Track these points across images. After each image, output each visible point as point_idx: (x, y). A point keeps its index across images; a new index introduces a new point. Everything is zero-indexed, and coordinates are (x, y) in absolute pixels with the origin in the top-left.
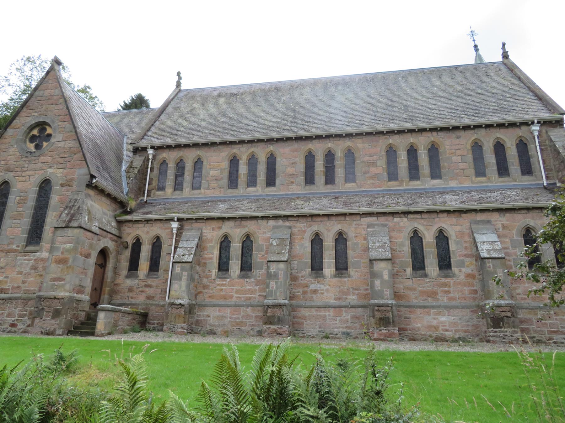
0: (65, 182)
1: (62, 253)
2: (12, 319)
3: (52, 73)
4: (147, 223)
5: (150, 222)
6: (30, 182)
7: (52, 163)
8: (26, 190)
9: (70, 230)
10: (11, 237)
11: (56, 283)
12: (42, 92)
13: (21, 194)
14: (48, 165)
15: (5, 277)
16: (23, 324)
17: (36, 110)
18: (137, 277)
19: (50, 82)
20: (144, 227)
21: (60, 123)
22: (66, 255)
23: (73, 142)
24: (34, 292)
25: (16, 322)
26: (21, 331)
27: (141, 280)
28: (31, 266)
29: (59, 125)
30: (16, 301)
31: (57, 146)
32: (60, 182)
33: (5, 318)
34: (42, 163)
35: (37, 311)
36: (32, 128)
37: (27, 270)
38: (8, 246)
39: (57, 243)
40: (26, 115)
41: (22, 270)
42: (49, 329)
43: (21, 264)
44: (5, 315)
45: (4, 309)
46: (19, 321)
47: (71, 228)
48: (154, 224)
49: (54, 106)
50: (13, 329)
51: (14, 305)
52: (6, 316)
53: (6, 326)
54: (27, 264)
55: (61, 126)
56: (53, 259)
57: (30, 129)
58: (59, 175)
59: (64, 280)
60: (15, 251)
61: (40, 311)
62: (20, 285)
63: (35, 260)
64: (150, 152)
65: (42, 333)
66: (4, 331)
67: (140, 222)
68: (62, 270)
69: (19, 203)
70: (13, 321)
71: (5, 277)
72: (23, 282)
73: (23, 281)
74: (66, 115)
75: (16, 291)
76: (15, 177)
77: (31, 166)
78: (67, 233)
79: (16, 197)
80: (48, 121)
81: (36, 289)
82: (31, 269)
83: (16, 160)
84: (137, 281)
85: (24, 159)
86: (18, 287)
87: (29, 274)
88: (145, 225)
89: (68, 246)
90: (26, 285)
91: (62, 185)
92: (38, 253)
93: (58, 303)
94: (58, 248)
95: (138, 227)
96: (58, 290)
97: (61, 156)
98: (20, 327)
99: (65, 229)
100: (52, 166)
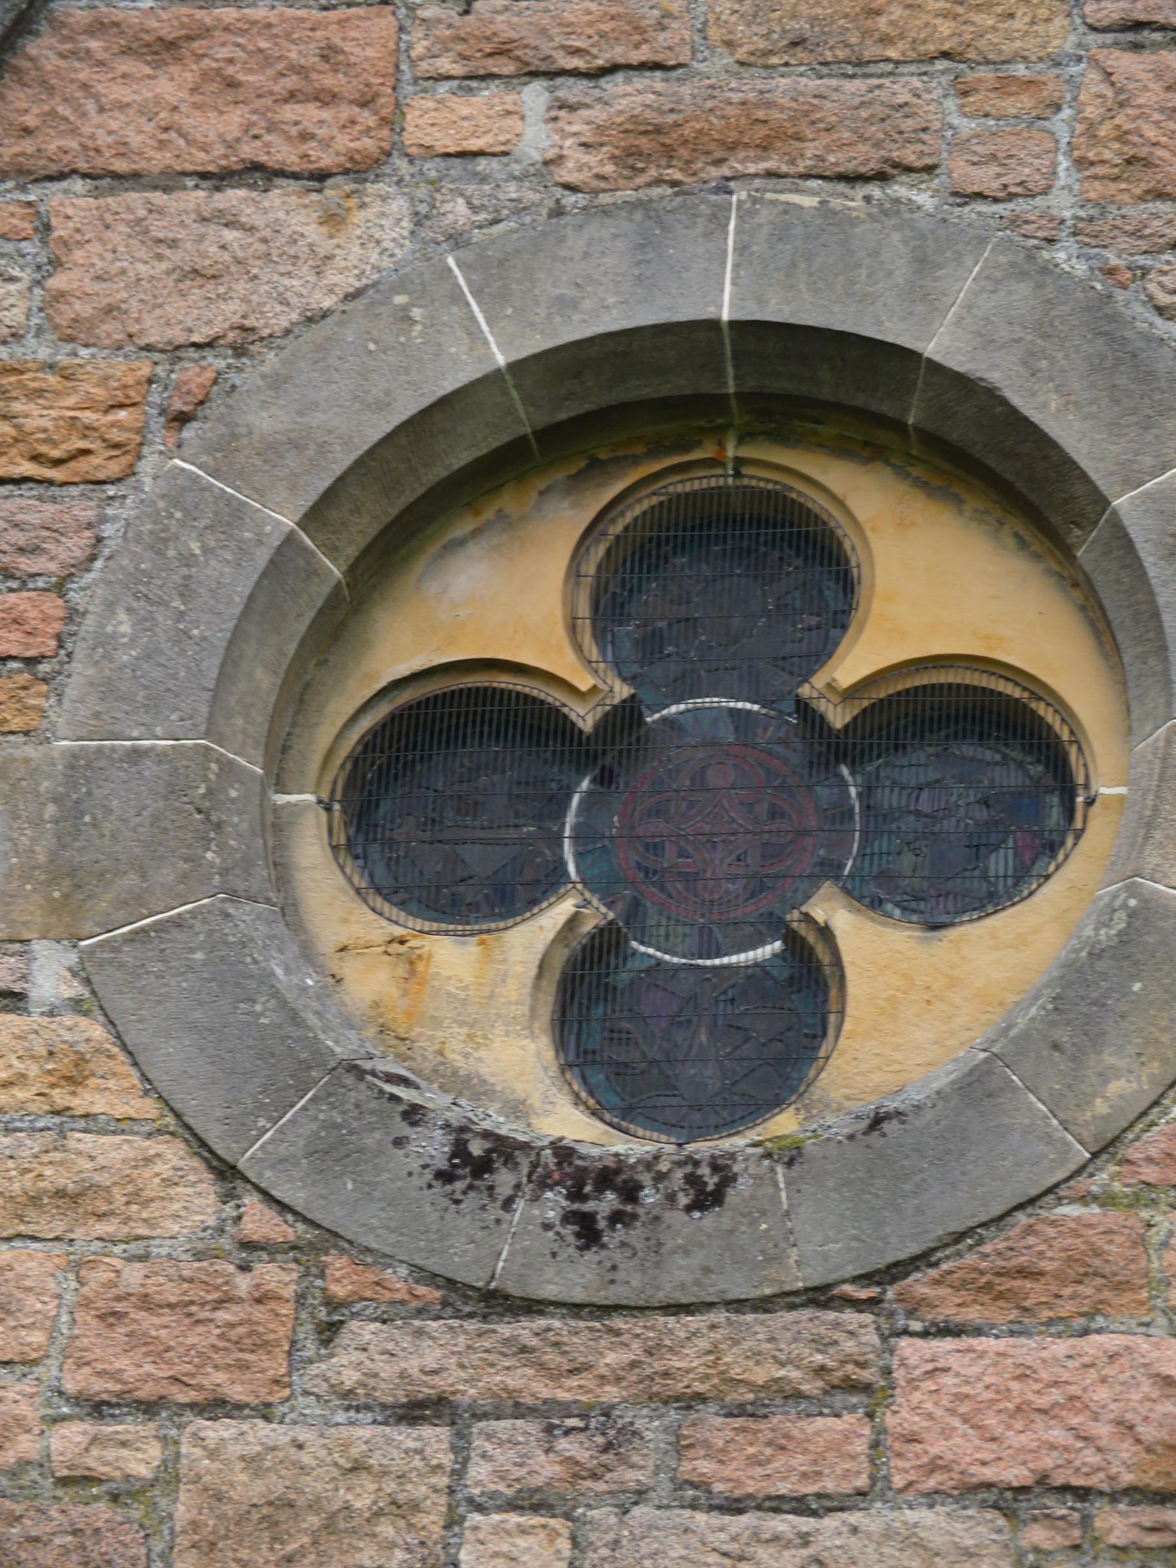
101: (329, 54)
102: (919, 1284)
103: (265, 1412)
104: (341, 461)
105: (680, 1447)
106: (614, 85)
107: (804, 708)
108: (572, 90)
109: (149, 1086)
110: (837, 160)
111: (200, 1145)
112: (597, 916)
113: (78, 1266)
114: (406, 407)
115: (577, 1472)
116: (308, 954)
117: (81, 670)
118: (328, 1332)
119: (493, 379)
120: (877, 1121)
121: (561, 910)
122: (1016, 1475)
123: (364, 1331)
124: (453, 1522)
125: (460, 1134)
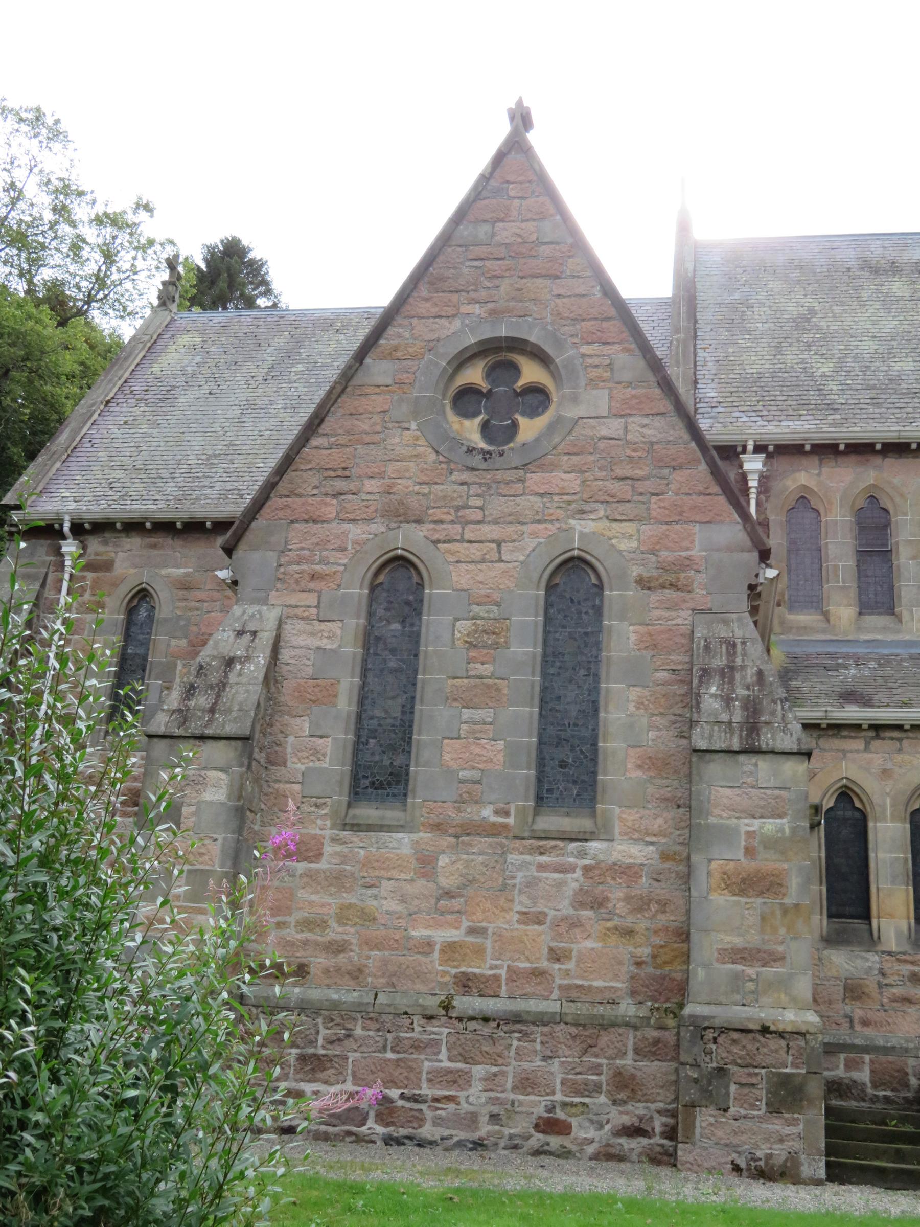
0: (655, 573)
1: (749, 851)
2: (545, 1101)
3: (514, 158)
4: (877, 737)
5: (888, 734)
6: (502, 565)
7: (585, 496)
8: (496, 596)
9: (763, 765)
10: (465, 774)
11: (751, 971)
12: (485, 228)
13: (476, 609)
14: (569, 503)
15: (472, 931)
16: (592, 1122)
17: (472, 295)
18: (871, 941)
19: (512, 194)
20: (867, 749)
21: (585, 349)
22: (768, 862)
23: (659, 422)
24: (608, 995)
25: (560, 1114)
26: (590, 1150)
27: (890, 953)
28: (576, 894)
29: (583, 356)
30: (546, 1029)
31: (589, 432)
32: (635, 571)
33: (512, 1096)
34: (542, 495)
35: (696, 1081)
36: (463, 360)
37: (566, 908)
38: (459, 810)
39: (716, 811)
40: (435, 310)
41: (541, 907)
42: (769, 1157)
43: (531, 883)
44: (509, 1085)
45: (500, 1061)
46: (574, 1110)
47: (768, 757)
48: (905, 743)
49: (548, 282)
50: (555, 1141)
51: (538, 1047)
52: (515, 1088)
53: (520, 1126)
54: (560, 885)
55: (596, 361)
56: (717, 876)
57: (455, 364)
58: (624, 545)
59: (779, 959)
60: (494, 830)
61: (710, 1083)
62: (544, 964)
63: (587, 869)
64: (753, 464)
65: (737, 1169)
66: (515, 1147)
67: (845, 733)
68: (763, 919)
69: (471, 645)
70: (551, 1109)
71: (472, 931)
72: (556, 956)
73: (551, 950)
74: (607, 319)
75: (529, 989)
76: (436, 542)
77: (497, 506)
78: (751, 773)
79: (458, 619)
80: (532, 339)
81: (619, 985)
82: (580, 904)
83: (426, 479)
84: (874, 958)
85: (456, 476)
86: (538, 974)
87: (575, 924)
88: (867, 744)
89: (770, 826)
90: (571, 965)
91: (644, 584)
92: (594, 845)
93: (783, 1052)
94: (727, 835)
95: (845, 752)
96: (764, 1000)
97: (619, 472)
98: (582, 1135)
99: (742, 758)
100: (586, 507)
101: (450, 300)
102: (529, 466)
103: (442, 484)
104: (451, 356)
105: (498, 488)
106: (488, 304)
107: (514, 390)
108: (482, 305)
109: (427, 441)
110: (519, 314)
111: (433, 448)
112: (486, 417)
113: (417, 465)
114: (461, 348)
115: (484, 491)
116: (447, 422)
117: (417, 385)
118: (451, 473)
119: (472, 345)
120: (524, 445)
121: (481, 417)
122: (542, 492)
123: (456, 473)
124: (468, 498)
125: (468, 447)
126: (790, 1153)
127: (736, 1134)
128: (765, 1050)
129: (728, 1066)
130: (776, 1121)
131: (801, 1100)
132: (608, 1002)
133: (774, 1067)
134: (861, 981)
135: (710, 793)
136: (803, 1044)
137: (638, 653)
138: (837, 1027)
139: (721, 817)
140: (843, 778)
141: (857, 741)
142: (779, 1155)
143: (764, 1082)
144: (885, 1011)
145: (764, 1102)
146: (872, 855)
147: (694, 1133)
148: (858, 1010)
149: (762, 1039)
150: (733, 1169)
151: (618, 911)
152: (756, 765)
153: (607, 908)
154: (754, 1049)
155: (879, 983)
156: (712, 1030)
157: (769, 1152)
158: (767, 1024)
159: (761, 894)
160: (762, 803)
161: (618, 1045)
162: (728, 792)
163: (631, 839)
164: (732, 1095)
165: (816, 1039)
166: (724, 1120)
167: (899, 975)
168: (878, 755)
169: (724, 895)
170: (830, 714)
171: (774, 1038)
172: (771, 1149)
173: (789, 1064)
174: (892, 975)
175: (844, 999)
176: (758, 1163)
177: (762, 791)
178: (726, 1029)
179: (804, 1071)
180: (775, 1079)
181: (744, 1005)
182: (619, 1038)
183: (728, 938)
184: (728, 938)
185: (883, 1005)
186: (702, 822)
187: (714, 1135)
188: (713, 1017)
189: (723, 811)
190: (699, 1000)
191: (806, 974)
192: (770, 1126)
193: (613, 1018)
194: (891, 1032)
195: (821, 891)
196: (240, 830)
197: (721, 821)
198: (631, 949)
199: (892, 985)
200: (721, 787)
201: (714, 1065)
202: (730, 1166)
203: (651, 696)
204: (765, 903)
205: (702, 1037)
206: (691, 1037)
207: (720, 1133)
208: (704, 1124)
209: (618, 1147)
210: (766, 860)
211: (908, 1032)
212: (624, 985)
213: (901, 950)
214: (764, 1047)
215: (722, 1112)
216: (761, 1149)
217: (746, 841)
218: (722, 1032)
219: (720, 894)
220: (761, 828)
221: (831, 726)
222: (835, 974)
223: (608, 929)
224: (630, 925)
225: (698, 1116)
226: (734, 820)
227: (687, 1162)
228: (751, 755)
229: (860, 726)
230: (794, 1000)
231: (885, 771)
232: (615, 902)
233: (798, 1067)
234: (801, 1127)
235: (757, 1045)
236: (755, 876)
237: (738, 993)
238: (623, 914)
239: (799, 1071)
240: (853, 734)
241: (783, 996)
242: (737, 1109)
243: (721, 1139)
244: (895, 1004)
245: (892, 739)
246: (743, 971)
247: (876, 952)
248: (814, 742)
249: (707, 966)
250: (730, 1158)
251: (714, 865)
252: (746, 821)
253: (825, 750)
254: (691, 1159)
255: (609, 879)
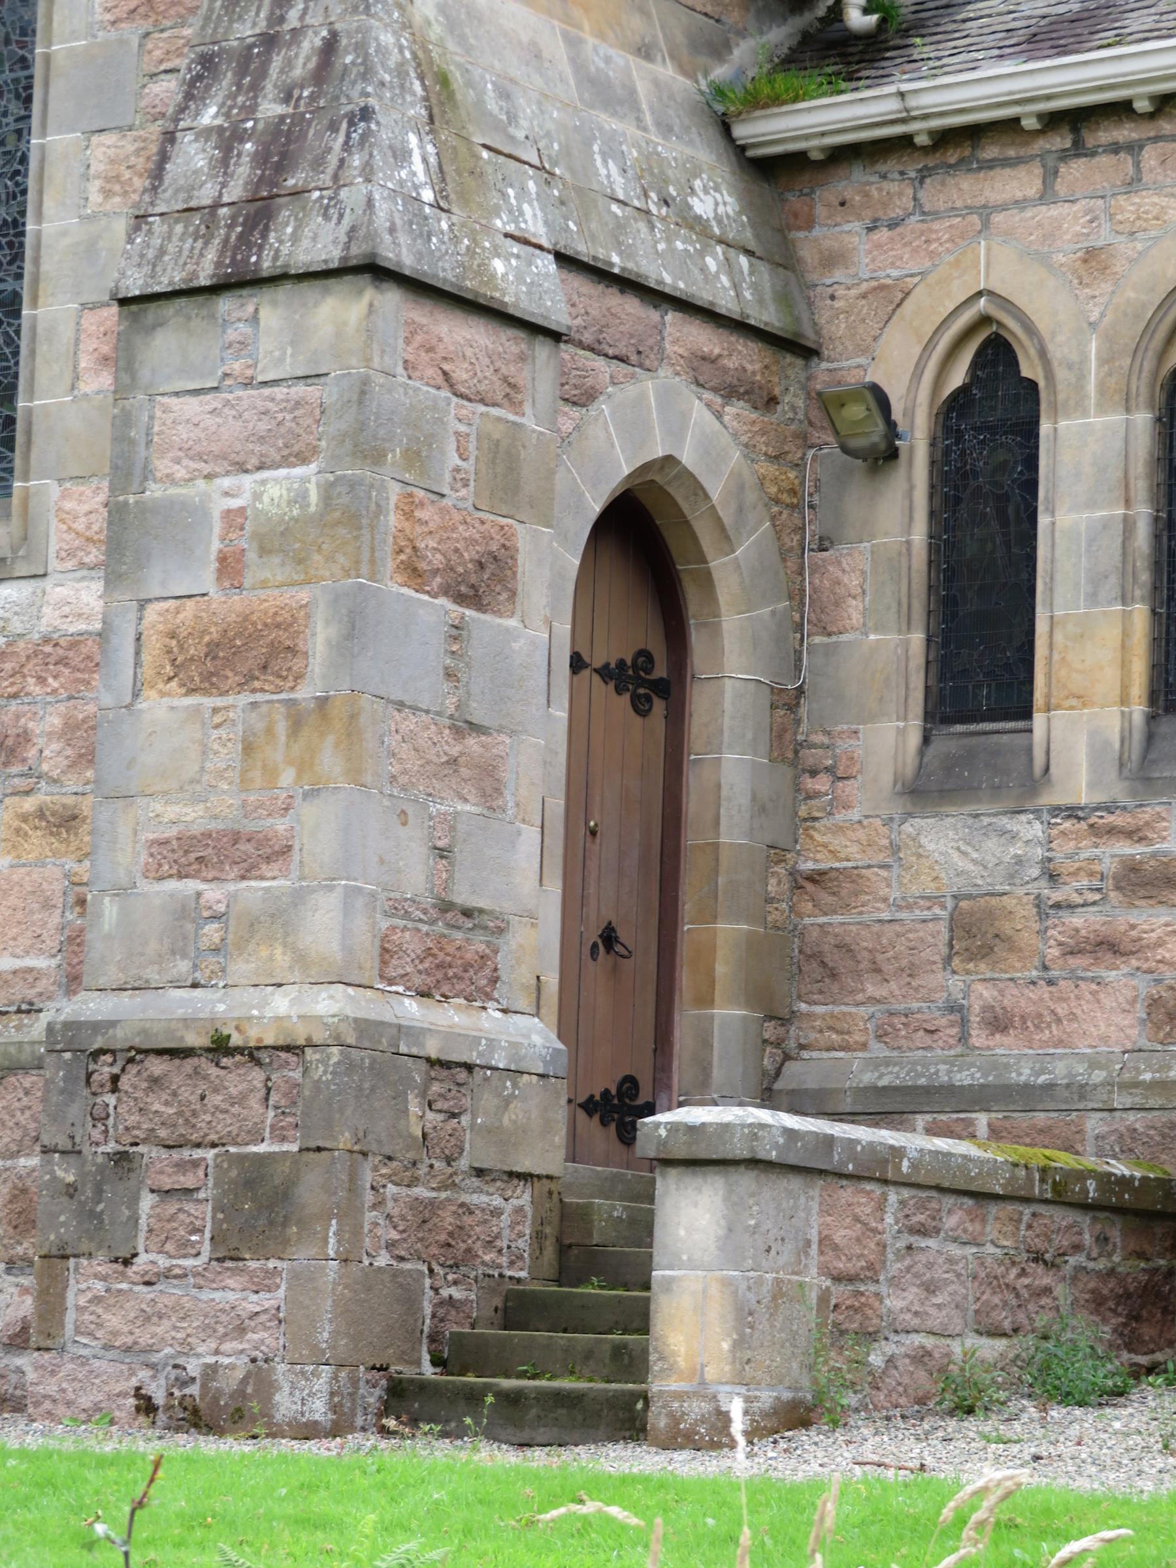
4: (1079, 150)
11: (214, 894)
20: (1047, 195)
27: (1072, 812)
35: (71, 1191)
39: (162, 466)
42: (211, 1371)
47: (283, 292)
48: (1150, 156)
56: (154, 645)
65: (146, 1407)
67: (990, 152)
68: (248, 749)
84: (1030, 829)
88: (1050, 176)
93: (255, 1102)
95: (986, 212)
96: (241, 968)
99: (225, 304)
126: (254, 1360)
127: (148, 1319)
128: (216, 1099)
129: (140, 1149)
130: (231, 1282)
131: (285, 1224)
132: (19, 1011)
133: (236, 1144)
134: (994, 901)
135: (152, 418)
136: (296, 1075)
137: (113, 34)
138: (928, 1040)
139: (170, 479)
140: (980, 294)
141: (1021, 172)
142: (232, 1367)
143: (210, 1184)
144: (1051, 982)
145: (208, 1235)
146: (1043, 520)
147: (62, 1325)
148: (979, 987)
149: (213, 1071)
150: (138, 1409)
151: (45, 767)
152: (255, 319)
153: (24, 760)
154: (194, 1098)
155: (1039, 902)
156: (108, 1058)
157: (211, 1360)
158: (226, 1032)
159: (247, 682)
160: (263, 426)
161: (22, 1118)
162: (192, 406)
163: (82, 565)
164: (143, 1221)
165: (324, 1062)
166: (124, 1286)
167: (1091, 874)
168: (1076, 207)
169: (168, 694)
170: (912, 102)
171: (238, 1065)
172: (217, 1352)
173: (267, 1135)
174: (1074, 874)
175: (948, 960)
176: (187, 1391)
177: (267, 391)
178: (140, 1051)
179: (294, 1148)
180: (234, 1173)
181: (195, 985)
182: (26, 1101)
183: (172, 812)
184: (172, 812)
185: (1045, 968)
186: (131, 499)
187: (100, 1325)
188: (113, 1024)
189: (178, 461)
190: (102, 982)
191: (331, 888)
192: (217, 1295)
193: (12, 1050)
194: (1060, 1043)
195: (906, 644)
196: (796, 596)
197: (173, 491)
198: (70, 864)
199: (1071, 907)
200: (177, 394)
201: (111, 1147)
202: (132, 1401)
203: (137, 152)
204: (254, 705)
205: (89, 1076)
206: (65, 1079)
207: (113, 1321)
208: (82, 1301)
209: (14, 1378)
210: (264, 585)
211: (1105, 1039)
212: (54, 962)
213: (1100, 797)
214: (216, 1090)
215: (119, 1267)
216: (198, 1356)
217: (223, 540)
218: (131, 1060)
219: (162, 694)
220: (257, 496)
221: (945, 138)
222: (930, 889)
223: (25, 818)
224: (70, 800)
225: (72, 1282)
226: (201, 483)
227: (45, 1397)
228: (245, 292)
229: (1013, 123)
230: (301, 959)
231: (1090, 255)
232: (41, 742)
233: (283, 1139)
234: (281, 1292)
235: (203, 1086)
236: (239, 634)
237: (184, 956)
238: (55, 774)
239: (286, 1147)
240: (1011, 153)
241: (278, 951)
242: (152, 1256)
243: (115, 1334)
244: (1073, 962)
245: (1115, 148)
246: (199, 895)
247: (1037, 812)
248: (910, 192)
249: (122, 891)
250: (134, 1382)
251: (152, 612)
252: (226, 482)
253: (936, 215)
254: (51, 1388)
255: (31, 684)
